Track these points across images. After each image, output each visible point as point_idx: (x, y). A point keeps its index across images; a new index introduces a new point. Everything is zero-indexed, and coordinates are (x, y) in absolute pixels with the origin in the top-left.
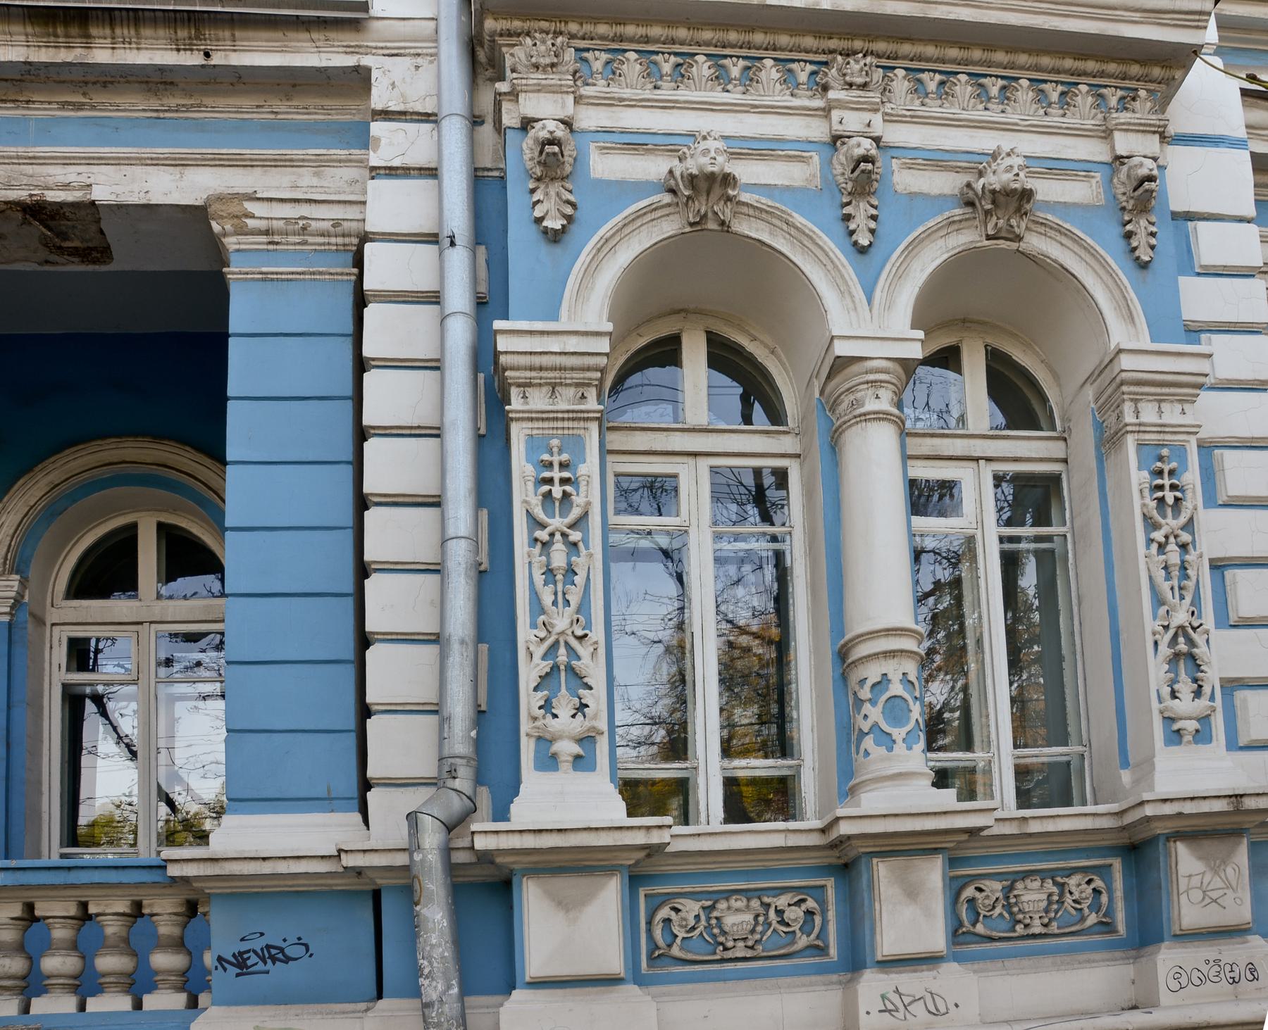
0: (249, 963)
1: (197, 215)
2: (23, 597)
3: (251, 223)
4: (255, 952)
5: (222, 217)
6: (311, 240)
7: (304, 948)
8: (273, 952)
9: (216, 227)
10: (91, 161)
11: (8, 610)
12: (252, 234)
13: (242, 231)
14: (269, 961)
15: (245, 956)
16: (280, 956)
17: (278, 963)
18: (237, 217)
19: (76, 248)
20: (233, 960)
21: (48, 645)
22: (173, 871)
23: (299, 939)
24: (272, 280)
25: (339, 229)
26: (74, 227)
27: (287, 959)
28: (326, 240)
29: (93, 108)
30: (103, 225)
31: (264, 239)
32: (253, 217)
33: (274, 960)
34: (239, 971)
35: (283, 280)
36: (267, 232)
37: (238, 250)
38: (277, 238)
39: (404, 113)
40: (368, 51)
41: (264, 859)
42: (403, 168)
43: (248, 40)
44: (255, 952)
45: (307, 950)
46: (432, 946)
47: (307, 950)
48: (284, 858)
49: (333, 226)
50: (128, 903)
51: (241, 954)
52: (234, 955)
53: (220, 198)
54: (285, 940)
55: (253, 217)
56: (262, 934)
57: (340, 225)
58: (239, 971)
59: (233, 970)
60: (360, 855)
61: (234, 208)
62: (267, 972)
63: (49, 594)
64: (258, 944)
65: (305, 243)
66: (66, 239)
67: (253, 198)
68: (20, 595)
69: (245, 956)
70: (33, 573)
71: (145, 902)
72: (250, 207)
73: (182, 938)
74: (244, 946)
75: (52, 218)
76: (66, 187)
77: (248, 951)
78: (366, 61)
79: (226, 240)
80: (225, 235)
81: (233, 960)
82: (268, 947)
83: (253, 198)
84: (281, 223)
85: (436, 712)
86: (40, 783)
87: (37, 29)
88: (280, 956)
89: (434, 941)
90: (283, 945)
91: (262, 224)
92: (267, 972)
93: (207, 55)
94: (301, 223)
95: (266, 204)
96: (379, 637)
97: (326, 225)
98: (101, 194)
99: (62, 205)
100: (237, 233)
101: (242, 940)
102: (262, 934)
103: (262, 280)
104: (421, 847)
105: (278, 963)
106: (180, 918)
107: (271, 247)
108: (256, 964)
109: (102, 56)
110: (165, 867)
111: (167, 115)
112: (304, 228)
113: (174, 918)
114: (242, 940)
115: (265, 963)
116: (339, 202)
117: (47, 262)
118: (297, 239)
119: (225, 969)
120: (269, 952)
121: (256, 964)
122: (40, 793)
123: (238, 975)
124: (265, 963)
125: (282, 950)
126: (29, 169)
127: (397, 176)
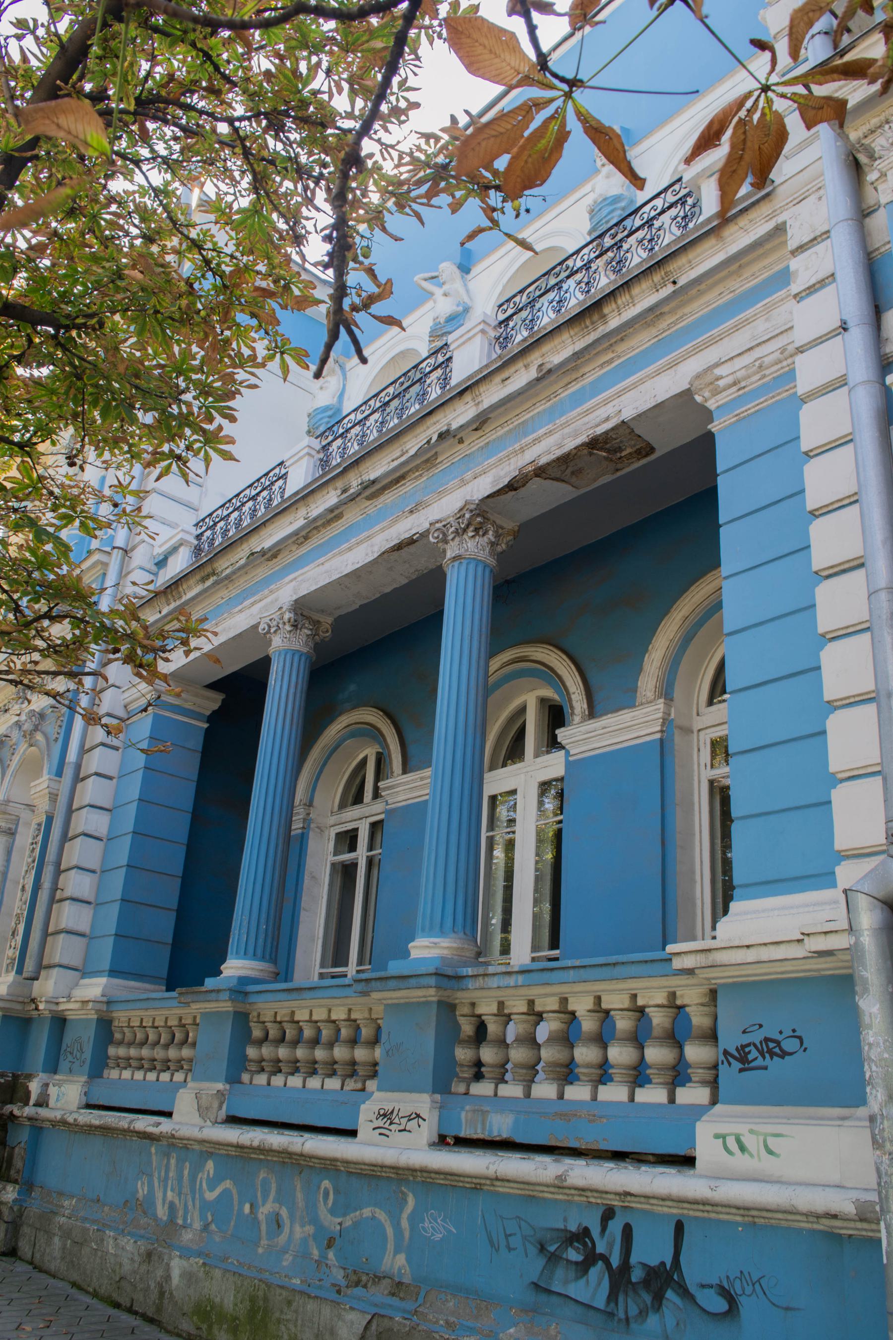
0: (750, 1057)
1: (686, 395)
2: (669, 715)
3: (721, 383)
4: (755, 1046)
5: (701, 389)
6: (767, 372)
7: (797, 1041)
8: (771, 1045)
9: (698, 399)
10: (619, 395)
11: (659, 728)
12: (724, 390)
13: (716, 392)
14: (767, 1055)
15: (747, 1050)
16: (777, 1050)
17: (775, 1058)
18: (711, 383)
19: (630, 454)
20: (736, 1054)
21: (696, 750)
22: (677, 963)
23: (794, 1031)
24: (744, 417)
25: (786, 353)
26: (621, 442)
27: (784, 1054)
28: (779, 366)
29: (619, 357)
30: (637, 432)
31: (735, 389)
32: (722, 377)
33: (772, 1054)
34: (741, 1066)
35: (752, 414)
36: (735, 384)
37: (718, 407)
38: (743, 384)
39: (815, 239)
40: (783, 209)
41: (748, 947)
42: (818, 282)
43: (699, 255)
44: (755, 1046)
45: (802, 1043)
46: (870, 1045)
47: (802, 1043)
48: (765, 944)
49: (782, 353)
50: (665, 994)
51: (743, 1047)
52: (737, 1049)
53: (698, 376)
54: (781, 1032)
55: (722, 377)
56: (761, 1026)
57: (785, 350)
58: (741, 1066)
59: (737, 1065)
60: (821, 938)
61: (709, 378)
62: (766, 1068)
63: (695, 706)
64: (757, 1037)
65: (764, 376)
66: (620, 450)
67: (717, 365)
68: (667, 714)
69: (747, 1050)
70: (677, 693)
71: (678, 993)
72: (718, 372)
73: (673, 1032)
74: (746, 1039)
75: (606, 443)
76: (607, 419)
77: (748, 1045)
78: (780, 219)
79: (708, 405)
80: (706, 401)
81: (736, 1054)
82: (767, 1040)
83: (717, 365)
84: (743, 371)
85: (878, 773)
86: (693, 872)
87: (576, 330)
88: (777, 1050)
89: (871, 1040)
90: (779, 1037)
91: (730, 380)
92: (766, 1068)
93: (674, 283)
94: (757, 364)
95: (729, 363)
96: (838, 703)
97: (777, 355)
98: (628, 414)
99: (606, 433)
100: (714, 395)
101: (744, 1032)
102: (761, 1026)
103: (737, 421)
104: (854, 928)
105: (775, 1058)
106: (706, 1009)
107: (741, 392)
108: (756, 1059)
109: (614, 323)
110: (671, 960)
111: (664, 335)
112: (760, 367)
113: (702, 1008)
114: (744, 1032)
115: (764, 1058)
116: (782, 333)
117: (617, 470)
118: (757, 377)
119: (730, 1064)
120: (767, 1046)
121: (756, 1059)
122: (693, 881)
123: (741, 1070)
124: (764, 1058)
125: (778, 1043)
126: (586, 419)
127: (816, 291)
